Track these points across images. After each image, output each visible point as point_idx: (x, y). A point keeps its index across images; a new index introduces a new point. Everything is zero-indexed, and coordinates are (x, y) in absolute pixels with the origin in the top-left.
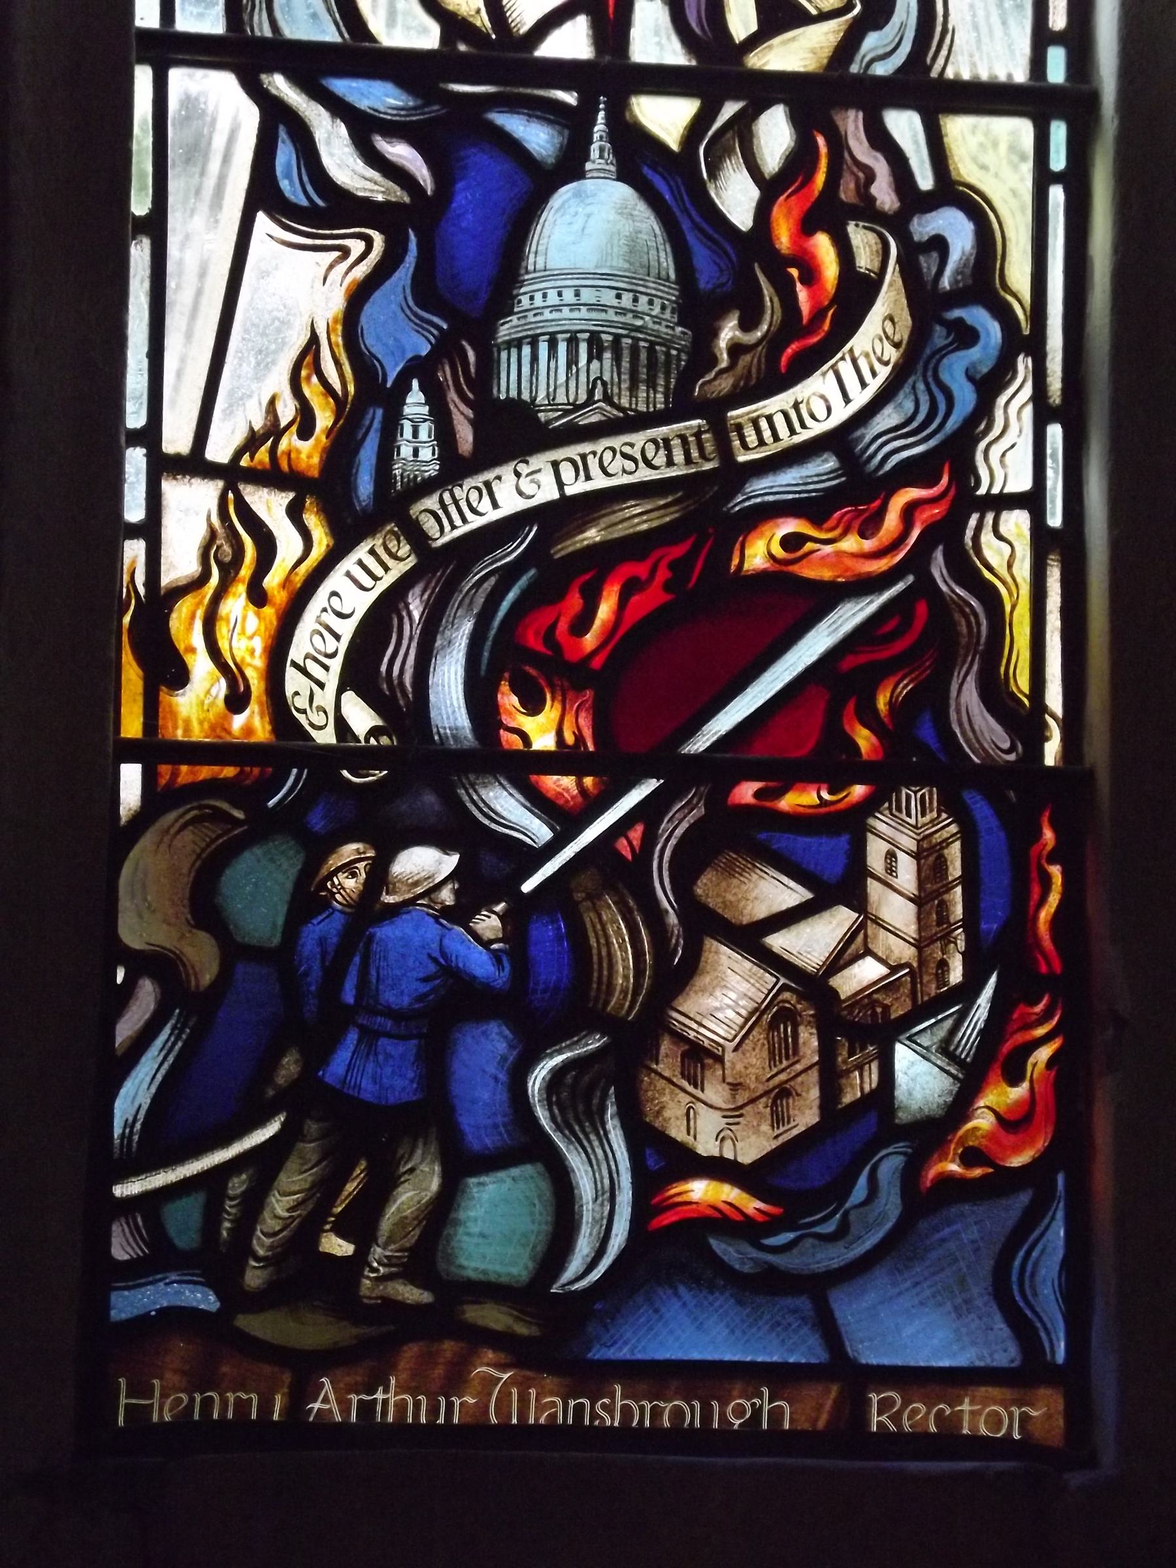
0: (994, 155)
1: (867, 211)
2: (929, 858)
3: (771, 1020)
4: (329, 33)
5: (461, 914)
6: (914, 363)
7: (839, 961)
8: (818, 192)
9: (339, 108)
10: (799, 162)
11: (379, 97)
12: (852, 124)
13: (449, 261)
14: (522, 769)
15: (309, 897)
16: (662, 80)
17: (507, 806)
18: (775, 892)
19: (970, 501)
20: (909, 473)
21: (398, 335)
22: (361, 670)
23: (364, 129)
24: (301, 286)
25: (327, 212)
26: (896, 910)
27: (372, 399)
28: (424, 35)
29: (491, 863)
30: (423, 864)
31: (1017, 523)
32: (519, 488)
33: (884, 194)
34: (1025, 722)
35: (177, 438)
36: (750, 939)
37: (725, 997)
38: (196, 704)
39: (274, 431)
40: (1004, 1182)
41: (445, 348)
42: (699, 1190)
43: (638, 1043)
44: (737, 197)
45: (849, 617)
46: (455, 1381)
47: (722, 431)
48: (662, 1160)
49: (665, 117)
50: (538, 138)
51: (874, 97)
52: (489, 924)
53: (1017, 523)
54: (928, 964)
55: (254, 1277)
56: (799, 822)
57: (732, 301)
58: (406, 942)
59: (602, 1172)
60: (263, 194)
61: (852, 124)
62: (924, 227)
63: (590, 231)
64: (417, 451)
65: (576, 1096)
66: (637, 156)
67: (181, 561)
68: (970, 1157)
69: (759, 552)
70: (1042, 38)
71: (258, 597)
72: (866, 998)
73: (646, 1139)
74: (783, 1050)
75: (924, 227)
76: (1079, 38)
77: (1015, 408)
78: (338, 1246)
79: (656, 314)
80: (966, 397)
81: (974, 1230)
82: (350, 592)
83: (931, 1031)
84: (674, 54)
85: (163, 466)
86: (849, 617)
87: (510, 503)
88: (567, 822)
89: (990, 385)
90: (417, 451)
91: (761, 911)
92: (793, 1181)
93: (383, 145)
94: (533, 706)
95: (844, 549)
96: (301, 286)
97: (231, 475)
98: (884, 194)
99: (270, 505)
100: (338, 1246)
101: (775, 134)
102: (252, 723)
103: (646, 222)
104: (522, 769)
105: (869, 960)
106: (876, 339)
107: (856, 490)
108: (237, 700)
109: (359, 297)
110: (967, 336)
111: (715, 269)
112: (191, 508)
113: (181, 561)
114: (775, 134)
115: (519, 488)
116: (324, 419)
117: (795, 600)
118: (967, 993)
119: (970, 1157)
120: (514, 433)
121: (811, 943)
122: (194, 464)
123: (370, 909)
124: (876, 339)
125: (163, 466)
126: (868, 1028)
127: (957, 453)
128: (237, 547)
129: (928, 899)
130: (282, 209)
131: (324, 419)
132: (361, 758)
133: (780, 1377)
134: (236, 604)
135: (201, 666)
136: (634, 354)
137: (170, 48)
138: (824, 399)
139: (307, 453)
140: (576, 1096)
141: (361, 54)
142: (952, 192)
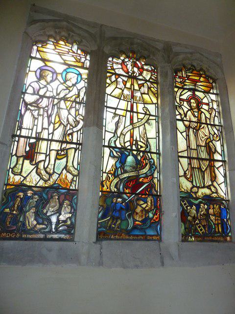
0: (154, 156)
1: (147, 159)
2: (151, 200)
3: (142, 211)
4: (114, 146)
5: (122, 203)
6: (150, 169)
7: (146, 207)
8: (144, 158)
9: (115, 150)
10: (143, 156)
11: (117, 150)
12: (146, 154)
13: (122, 160)
14: (126, 193)
15: (112, 202)
16: (134, 150)
17: (125, 196)
18: (142, 202)
19: (153, 178)
20: (150, 176)
21: (118, 165)
22: (116, 186)
23: (116, 152)
24: (112, 162)
25: (114, 157)
26: (149, 204)
27: (117, 169)
28: (120, 146)
29: (124, 200)
30: (119, 200)
31: (156, 179)
32: (126, 175)
33: (148, 158)
34: (157, 192)
35: (104, 171)
36: (140, 206)
37: (139, 209)
38: (105, 188)
39: (110, 170)
40: (156, 222)
41: (121, 166)
42: (137, 222)
43: (133, 212)
44: (139, 158)
45: (146, 185)
46: (121, 235)
47: (139, 172)
48: (135, 220)
49: (135, 153)
50: (127, 153)
51: (147, 152)
52: (124, 204)
53: (156, 179)
54: (151, 208)
55: (108, 228)
56: (143, 198)
57: (139, 165)
58: (118, 206)
59: (131, 221)
60: (110, 155)
61: (146, 154)
62: (150, 160)
63: (130, 159)
64: (119, 172)
65: (129, 216)
66: (133, 155)
67: (104, 179)
68: (154, 220)
69: (141, 180)
70: (157, 149)
71: (109, 181)
72: (147, 210)
73: (133, 219)
74: (142, 213)
75: (150, 160)
76: (159, 150)
77: (156, 172)
78: (114, 226)
79: (134, 165)
80: (153, 171)
81: (154, 225)
82: (115, 181)
83: (152, 212)
84: (135, 149)
85: (103, 172)
86: (146, 185)
87: (125, 176)
88: (129, 197)
89: (154, 170)
90: (119, 172)
91: (141, 204)
92: (143, 222)
93: (56, 128)
94: (127, 189)
95: (146, 180)
96: (112, 162)
97: (108, 173)
98: (148, 158)
99: (110, 175)
100: (114, 226)
101: (141, 154)
102: (108, 190)
103: (134, 159)
104: (126, 193)
105: (148, 95)
106: (148, 167)
107: (146, 177)
108: (107, 188)
109: (116, 162)
110: (153, 167)
111: (138, 162)
112: (105, 175)
113: (104, 179)
114: (141, 154)
115: (126, 175)
116: (114, 170)
117: (143, 184)
118: (154, 210)
119: (154, 220)
120: (126, 172)
121: (144, 206)
122: (105, 172)
123: (116, 203)
124: (148, 167)
125: (103, 172)
126: (148, 212)
127: (152, 175)
128: (108, 178)
129: (151, 203)
130: (111, 157)
131: (114, 170)
132: (115, 192)
133: (142, 235)
134: (108, 182)
135: (105, 186)
136: (134, 168)
137: (104, 146)
138: (144, 171)
139: (112, 172)
140: (129, 216)
141: (116, 147)
142: (152, 158)
